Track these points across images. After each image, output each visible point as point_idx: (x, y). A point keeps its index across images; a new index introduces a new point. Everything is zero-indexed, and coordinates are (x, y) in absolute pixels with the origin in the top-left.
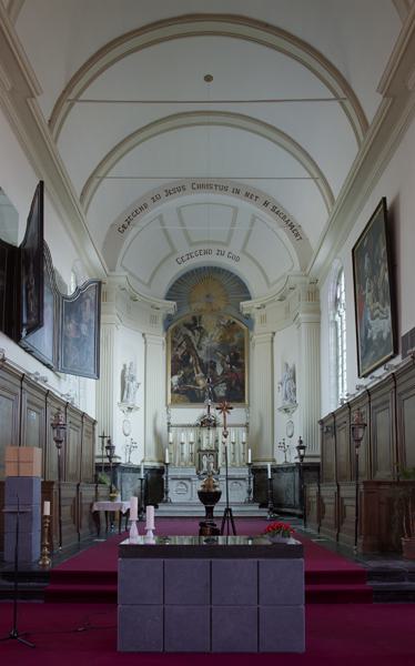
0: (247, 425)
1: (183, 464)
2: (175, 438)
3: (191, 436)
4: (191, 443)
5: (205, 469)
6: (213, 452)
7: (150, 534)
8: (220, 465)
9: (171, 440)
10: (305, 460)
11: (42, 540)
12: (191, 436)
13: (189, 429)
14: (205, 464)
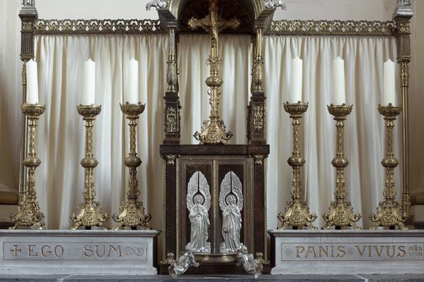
0: (396, 30)
1: (90, 214)
2: (61, 86)
3: (135, 76)
4: (132, 112)
5: (199, 247)
6: (239, 156)
7: (205, 21)
8: (271, 224)
9: (33, 99)
10: (398, 199)
11: (85, 181)
12: (135, 76)
13: (124, 45)
14: (199, 213)
